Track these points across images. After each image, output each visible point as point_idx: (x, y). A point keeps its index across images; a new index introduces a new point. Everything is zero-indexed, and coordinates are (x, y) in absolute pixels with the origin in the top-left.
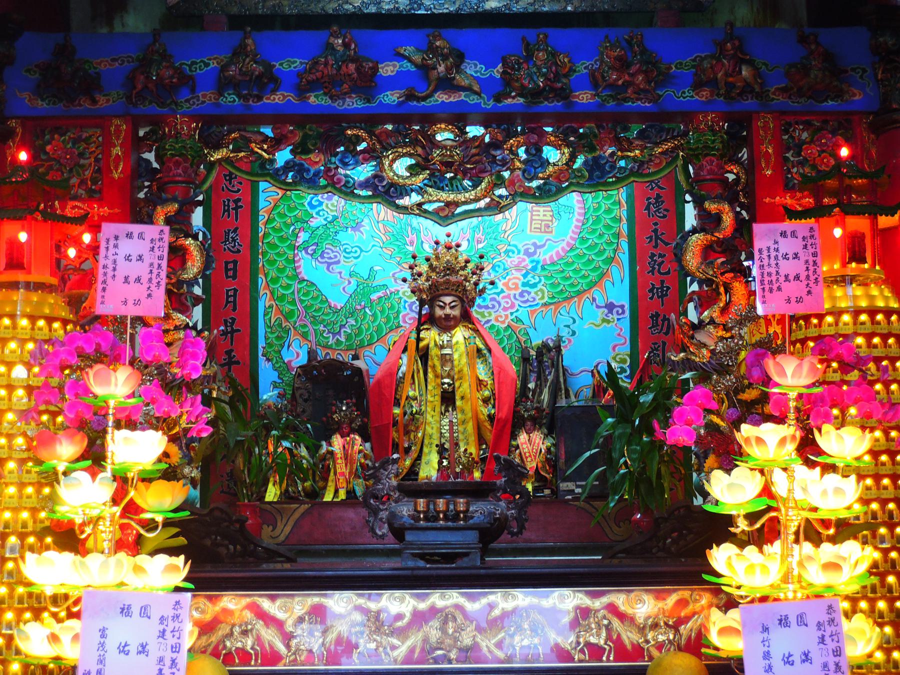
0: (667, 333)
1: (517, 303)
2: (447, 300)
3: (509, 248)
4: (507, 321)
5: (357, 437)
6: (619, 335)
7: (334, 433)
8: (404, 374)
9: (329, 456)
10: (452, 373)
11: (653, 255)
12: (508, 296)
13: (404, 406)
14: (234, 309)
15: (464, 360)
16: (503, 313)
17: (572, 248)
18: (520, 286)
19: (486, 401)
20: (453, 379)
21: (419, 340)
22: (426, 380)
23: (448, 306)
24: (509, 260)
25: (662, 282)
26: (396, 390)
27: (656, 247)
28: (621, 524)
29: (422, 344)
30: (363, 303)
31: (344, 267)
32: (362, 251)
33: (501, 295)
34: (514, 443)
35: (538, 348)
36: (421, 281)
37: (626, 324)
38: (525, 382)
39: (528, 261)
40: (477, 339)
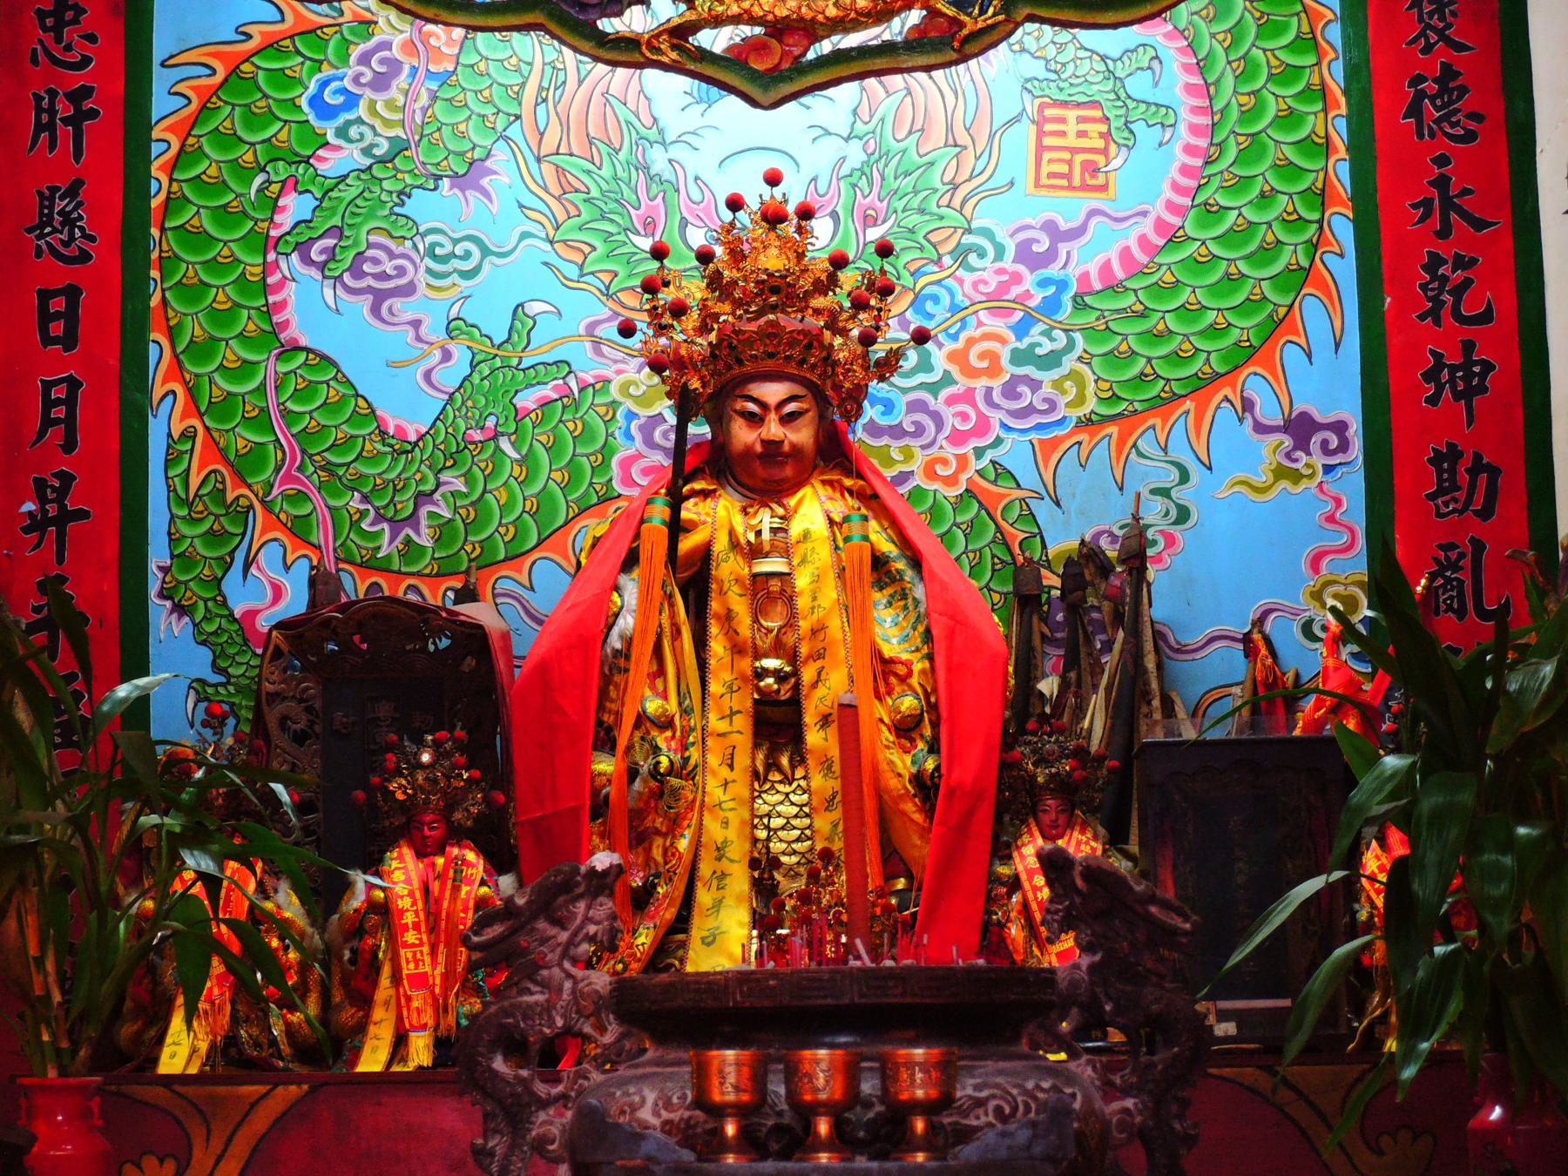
0: (1485, 513)
1: (996, 417)
2: (773, 392)
3: (968, 239)
4: (963, 477)
5: (471, 856)
6: (1331, 519)
7: (392, 844)
8: (628, 642)
9: (374, 918)
10: (790, 639)
11: (1435, 262)
12: (968, 396)
13: (629, 748)
14: (69, 446)
15: (830, 593)
16: (950, 452)
17: (1174, 238)
18: (1005, 361)
19: (905, 729)
20: (792, 657)
21: (677, 527)
22: (702, 665)
23: (774, 412)
24: (968, 277)
25: (1468, 347)
26: (603, 695)
27: (1444, 233)
28: (1385, 1141)
29: (687, 543)
30: (491, 422)
31: (429, 308)
32: (486, 252)
33: (945, 393)
34: (1003, 870)
35: (1069, 562)
36: (682, 332)
37: (1352, 485)
38: (1028, 672)
39: (1029, 281)
40: (873, 524)
